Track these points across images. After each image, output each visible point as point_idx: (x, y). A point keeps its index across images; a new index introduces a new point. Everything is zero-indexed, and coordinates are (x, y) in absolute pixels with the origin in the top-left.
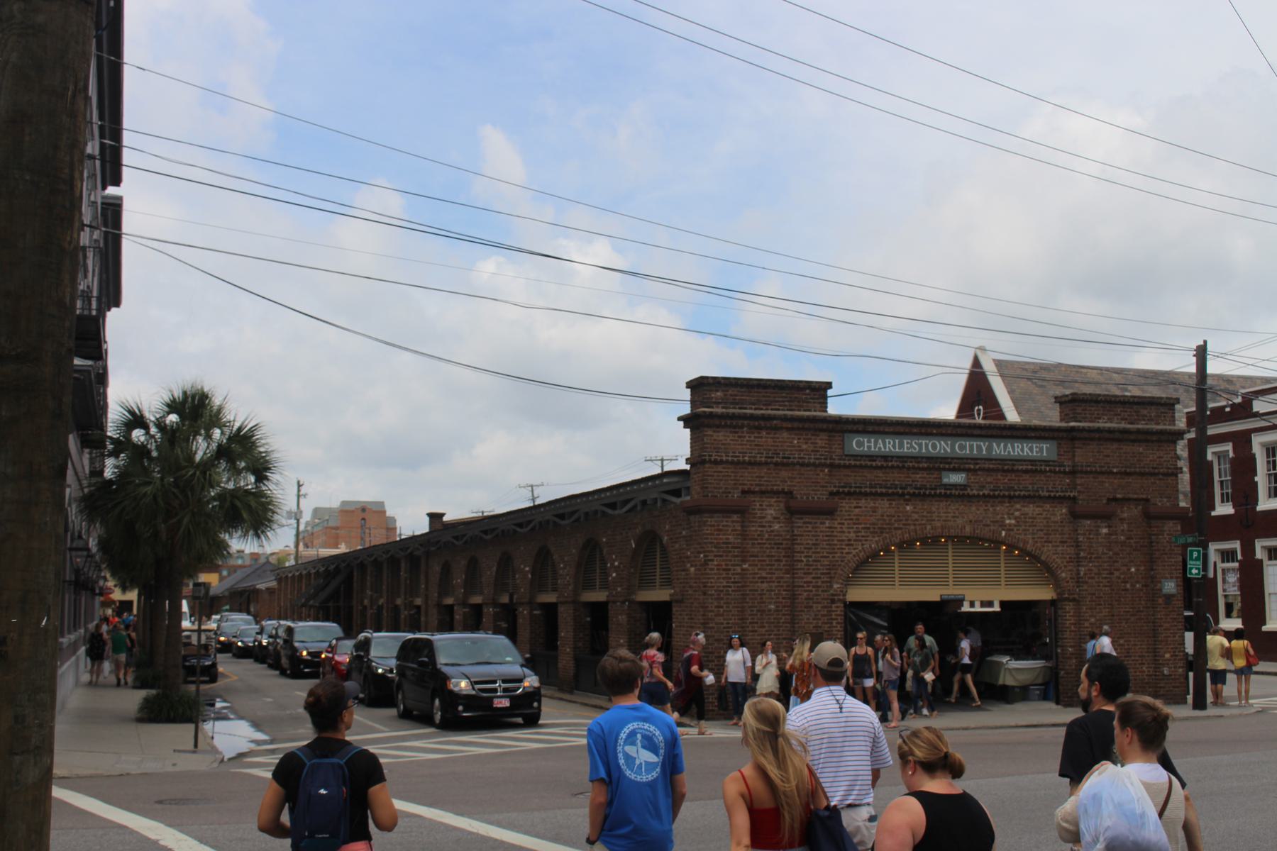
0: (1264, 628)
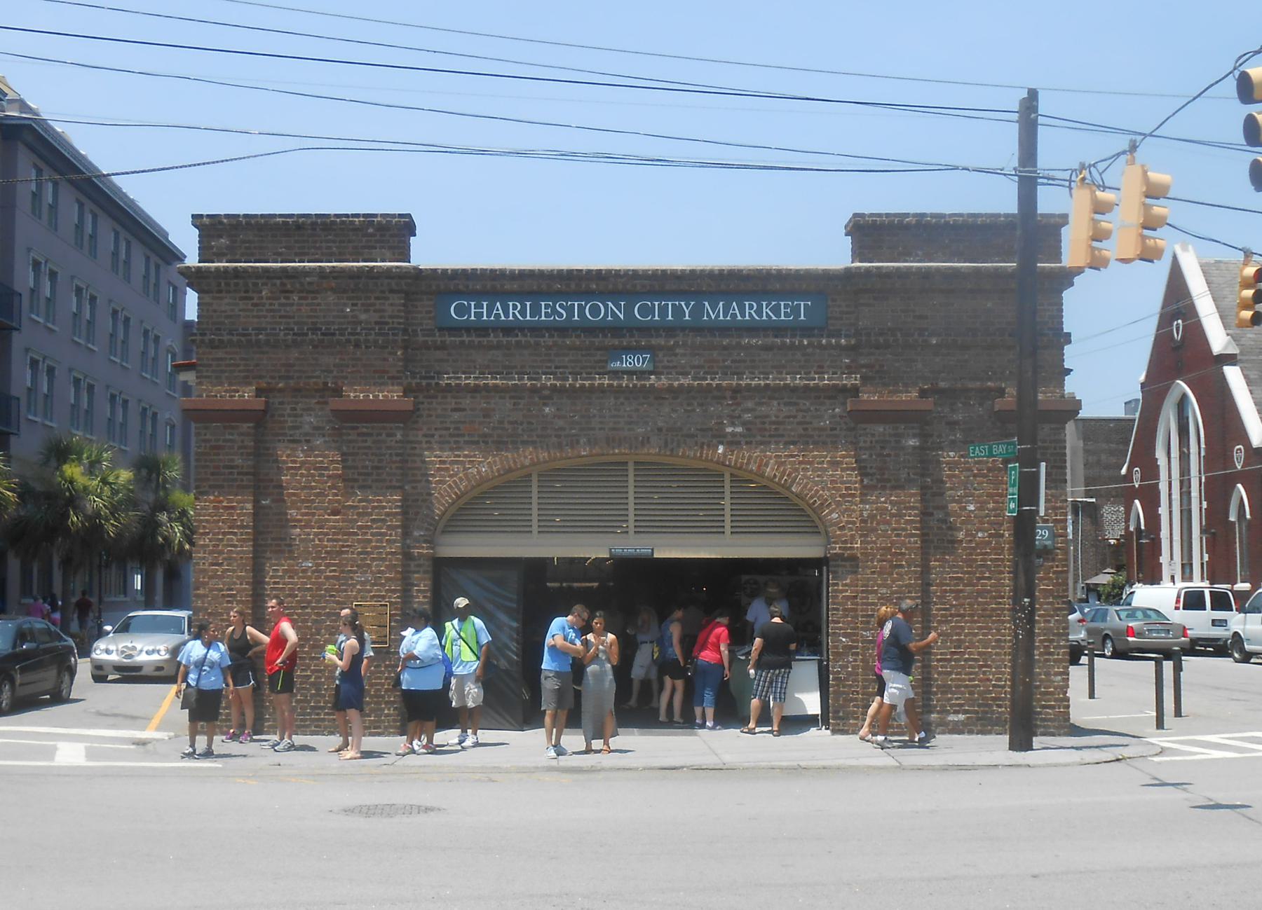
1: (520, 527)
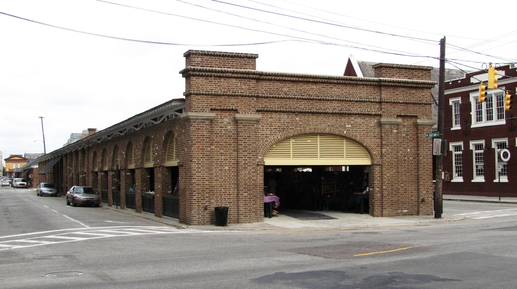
0: (472, 181)
1: (287, 155)
